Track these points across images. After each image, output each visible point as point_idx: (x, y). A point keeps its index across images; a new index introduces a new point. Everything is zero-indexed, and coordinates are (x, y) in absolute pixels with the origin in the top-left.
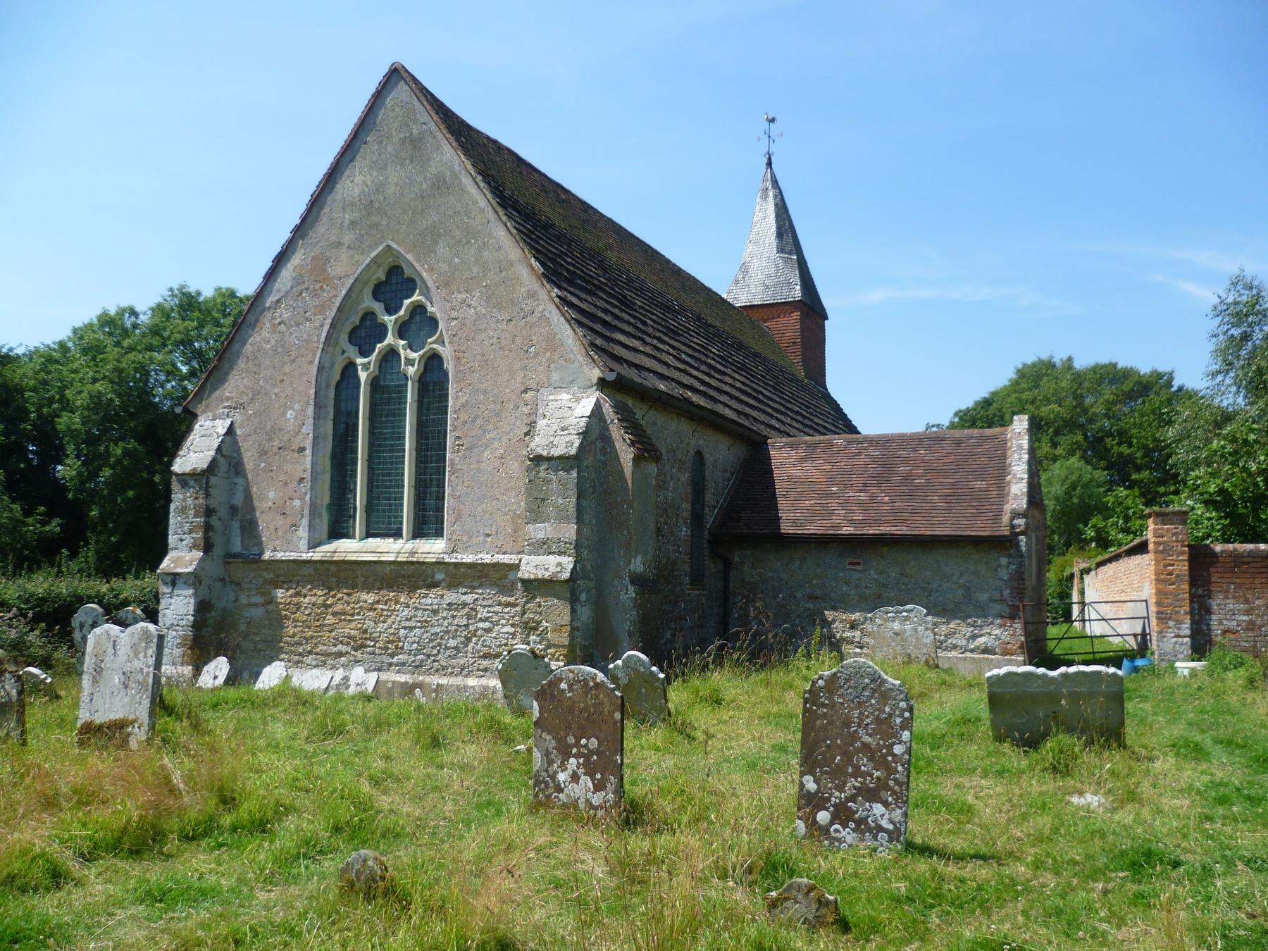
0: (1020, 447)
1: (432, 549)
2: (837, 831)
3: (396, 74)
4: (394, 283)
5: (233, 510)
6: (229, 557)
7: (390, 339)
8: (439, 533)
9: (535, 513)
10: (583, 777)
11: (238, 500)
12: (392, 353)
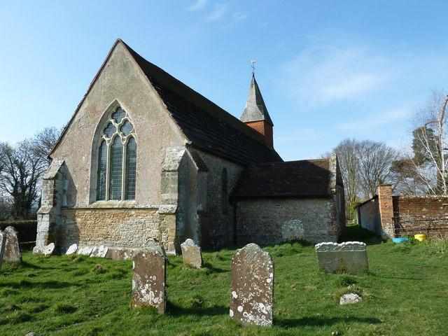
0: (334, 165)
1: (131, 203)
2: (245, 314)
3: (118, 42)
4: (116, 111)
5: (64, 191)
6: (63, 208)
7: (117, 132)
8: (133, 198)
9: (164, 190)
10: (151, 292)
11: (66, 188)
12: (117, 136)
